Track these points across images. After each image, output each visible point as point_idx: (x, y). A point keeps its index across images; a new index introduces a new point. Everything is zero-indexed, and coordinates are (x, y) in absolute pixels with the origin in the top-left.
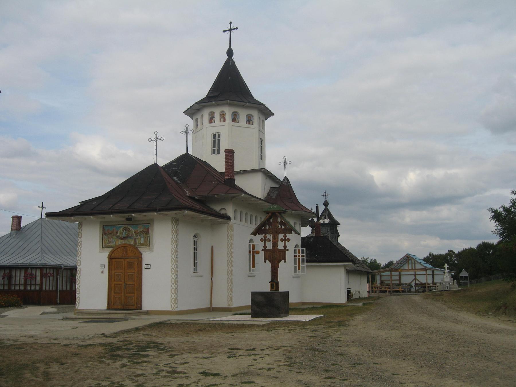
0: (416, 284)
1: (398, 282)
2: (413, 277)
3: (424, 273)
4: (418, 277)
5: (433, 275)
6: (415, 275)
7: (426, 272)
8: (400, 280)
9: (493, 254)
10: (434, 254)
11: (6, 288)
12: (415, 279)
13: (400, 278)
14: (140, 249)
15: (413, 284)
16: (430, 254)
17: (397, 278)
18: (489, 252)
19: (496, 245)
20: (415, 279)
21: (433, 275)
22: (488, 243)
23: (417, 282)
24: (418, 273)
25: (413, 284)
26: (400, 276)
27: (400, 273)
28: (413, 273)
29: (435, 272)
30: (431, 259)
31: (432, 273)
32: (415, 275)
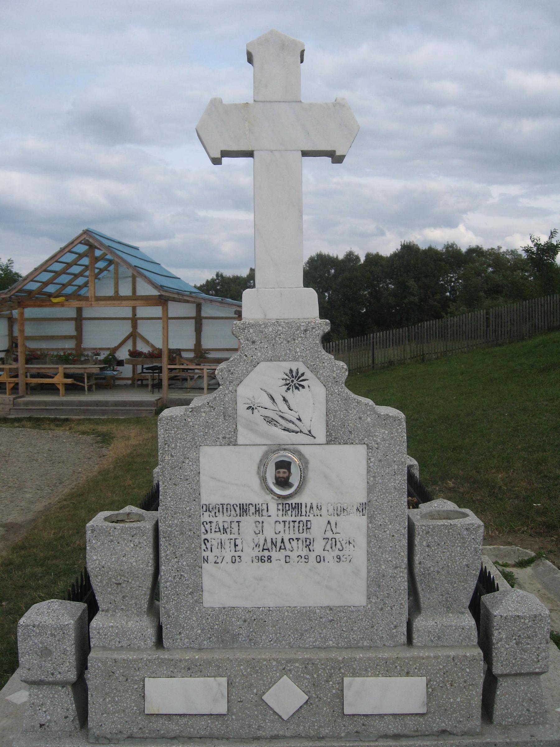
0: (134, 354)
1: (70, 345)
2: (127, 329)
3: (157, 311)
4: (143, 329)
5: (199, 321)
6: (134, 320)
7: (165, 311)
8: (79, 337)
9: (335, 276)
10: (224, 275)
11: (16, 313)
12: (134, 335)
13: (79, 328)
14: (44, 290)
15: (123, 354)
16: (217, 275)
17: (69, 329)
18: (329, 272)
19: (342, 261)
20: (134, 335)
21: (199, 321)
22: (328, 255)
23: (143, 348)
24: (143, 311)
25: (123, 354)
26: (79, 320)
27: (79, 310)
28: (127, 312)
29: (207, 311)
30: (218, 284)
31: (194, 314)
32: (134, 320)
